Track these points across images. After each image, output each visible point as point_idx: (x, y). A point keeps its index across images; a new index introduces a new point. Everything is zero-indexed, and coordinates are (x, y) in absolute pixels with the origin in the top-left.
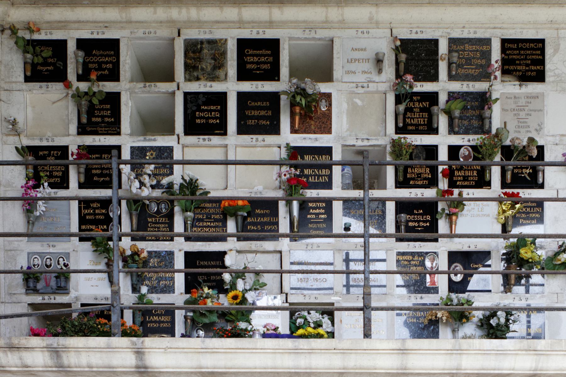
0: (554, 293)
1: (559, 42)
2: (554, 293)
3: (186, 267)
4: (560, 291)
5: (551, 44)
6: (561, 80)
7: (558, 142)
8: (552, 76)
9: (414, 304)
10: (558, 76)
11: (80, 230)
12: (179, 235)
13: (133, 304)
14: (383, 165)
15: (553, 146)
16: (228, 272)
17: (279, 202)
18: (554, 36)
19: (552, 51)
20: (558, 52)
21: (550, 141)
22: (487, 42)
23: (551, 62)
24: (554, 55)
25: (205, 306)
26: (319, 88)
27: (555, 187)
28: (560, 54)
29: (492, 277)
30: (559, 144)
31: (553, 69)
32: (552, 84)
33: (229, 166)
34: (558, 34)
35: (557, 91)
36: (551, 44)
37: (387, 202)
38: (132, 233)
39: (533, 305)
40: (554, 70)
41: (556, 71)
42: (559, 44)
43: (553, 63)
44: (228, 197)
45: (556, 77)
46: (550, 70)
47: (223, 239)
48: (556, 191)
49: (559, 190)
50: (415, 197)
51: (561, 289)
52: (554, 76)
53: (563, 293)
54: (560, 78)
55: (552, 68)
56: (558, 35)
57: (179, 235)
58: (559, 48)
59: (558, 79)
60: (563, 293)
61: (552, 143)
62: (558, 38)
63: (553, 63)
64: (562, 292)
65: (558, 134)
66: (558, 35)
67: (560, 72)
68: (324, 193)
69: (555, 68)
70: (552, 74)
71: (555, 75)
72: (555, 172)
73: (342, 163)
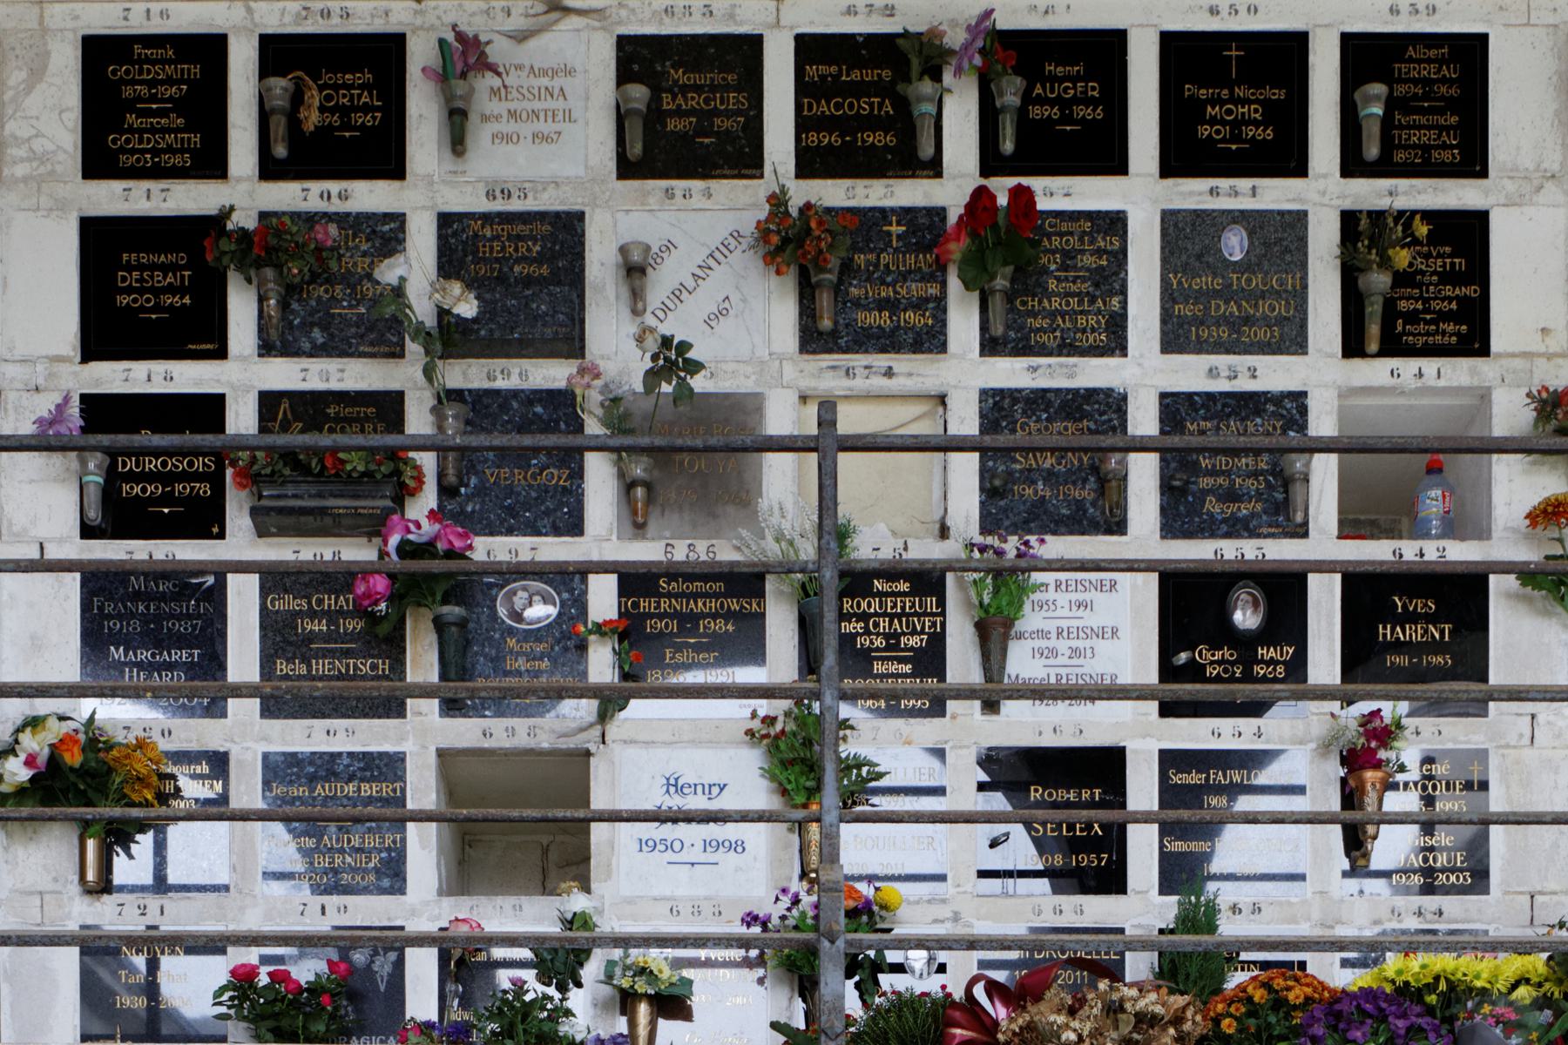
0: (31, 893)
1: (45, 44)
2: (31, 893)
3: (1163, 804)
4: (51, 887)
5: (18, 52)
6: (52, 173)
7: (41, 381)
8: (22, 160)
9: (1034, 930)
10: (42, 159)
11: (1168, 671)
12: (240, 691)
13: (1161, 931)
14: (745, 450)
15: (25, 395)
16: (281, 820)
17: (1311, 576)
18: (29, 26)
19: (23, 75)
20: (41, 80)
21: (12, 380)
22: (1291, 48)
23: (18, 114)
24: (29, 89)
25: (586, 934)
26: (416, 185)
27: (33, 533)
28: (51, 84)
29: (232, 833)
30: (46, 390)
31: (26, 135)
32: (22, 185)
33: (949, 454)
34: (42, 16)
35: (38, 209)
36: (18, 52)
37: (592, 578)
38: (989, 686)
39: (167, 927)
40: (29, 139)
41: (37, 145)
42: (48, 54)
43: (26, 118)
44: (60, 561)
45: (35, 164)
46: (16, 138)
47: (392, 707)
48: (38, 546)
49: (45, 545)
50: (1418, 559)
51: (56, 880)
52: (29, 160)
53: (60, 893)
54: (49, 167)
55: (25, 132)
56: (41, 23)
57: (425, 692)
58: (46, 67)
59: (42, 170)
60: (60, 893)
61: (21, 386)
62: (44, 30)
63: (26, 118)
64: (58, 887)
65: (44, 354)
66: (41, 23)
67: (50, 147)
68: (553, 549)
69: (34, 132)
70: (21, 152)
71: (33, 157)
72: (31, 481)
73: (1340, 446)
